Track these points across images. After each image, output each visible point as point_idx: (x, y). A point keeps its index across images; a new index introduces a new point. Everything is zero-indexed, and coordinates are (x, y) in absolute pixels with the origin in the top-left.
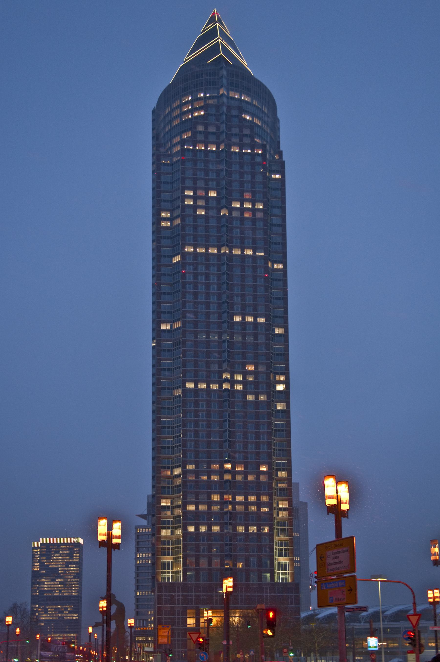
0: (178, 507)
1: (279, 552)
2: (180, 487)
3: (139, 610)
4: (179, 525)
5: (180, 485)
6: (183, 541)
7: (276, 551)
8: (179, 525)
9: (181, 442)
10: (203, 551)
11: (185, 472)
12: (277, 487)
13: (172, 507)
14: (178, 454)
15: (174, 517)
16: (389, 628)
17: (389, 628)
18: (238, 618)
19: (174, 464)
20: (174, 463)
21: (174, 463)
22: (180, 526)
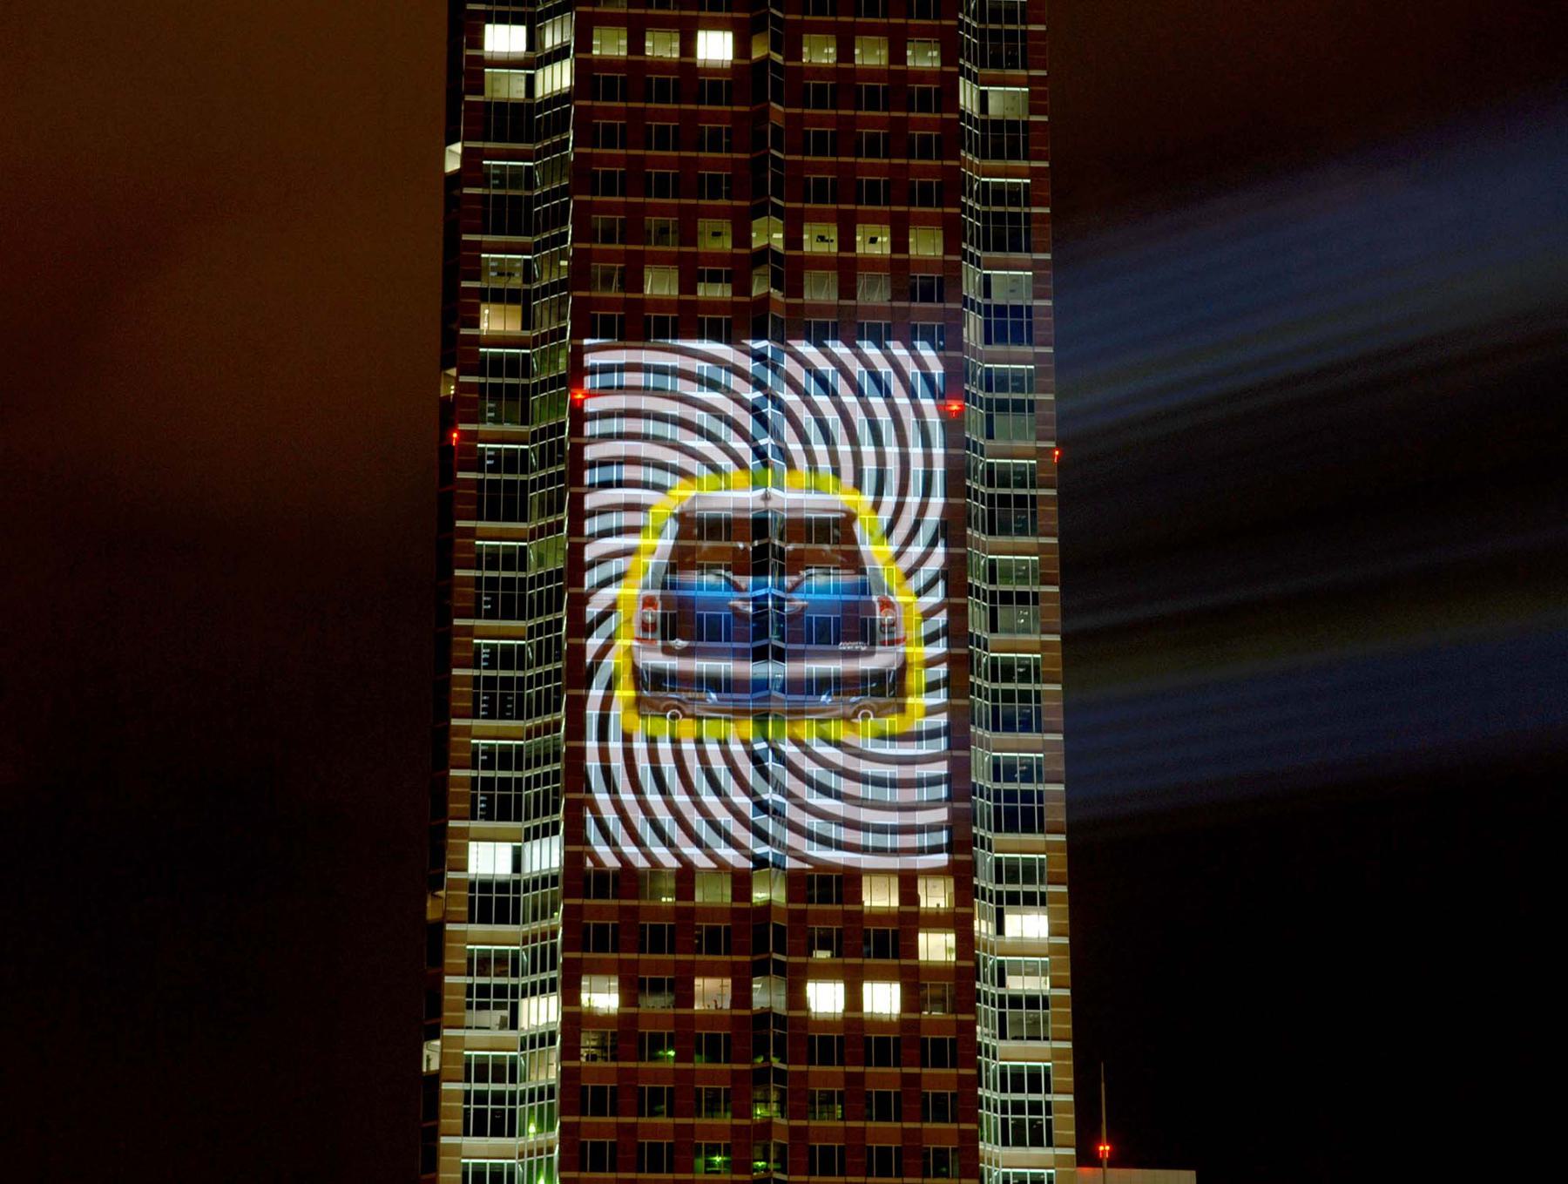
0: (543, 991)
1: (1004, 1121)
2: (551, 1096)
3: (506, 272)
4: (546, 976)
5: (551, 1089)
6: (563, 950)
7: (990, 1117)
8: (546, 976)
9: (563, 757)
10: (607, 281)
11: (575, 1021)
12: (1002, 991)
13: (516, 883)
14: (548, 718)
15: (524, 1039)
16: (1029, 613)
17: (1029, 613)
18: (773, 996)
19: (528, 767)
20: (529, 761)
21: (529, 761)
22: (553, 981)
